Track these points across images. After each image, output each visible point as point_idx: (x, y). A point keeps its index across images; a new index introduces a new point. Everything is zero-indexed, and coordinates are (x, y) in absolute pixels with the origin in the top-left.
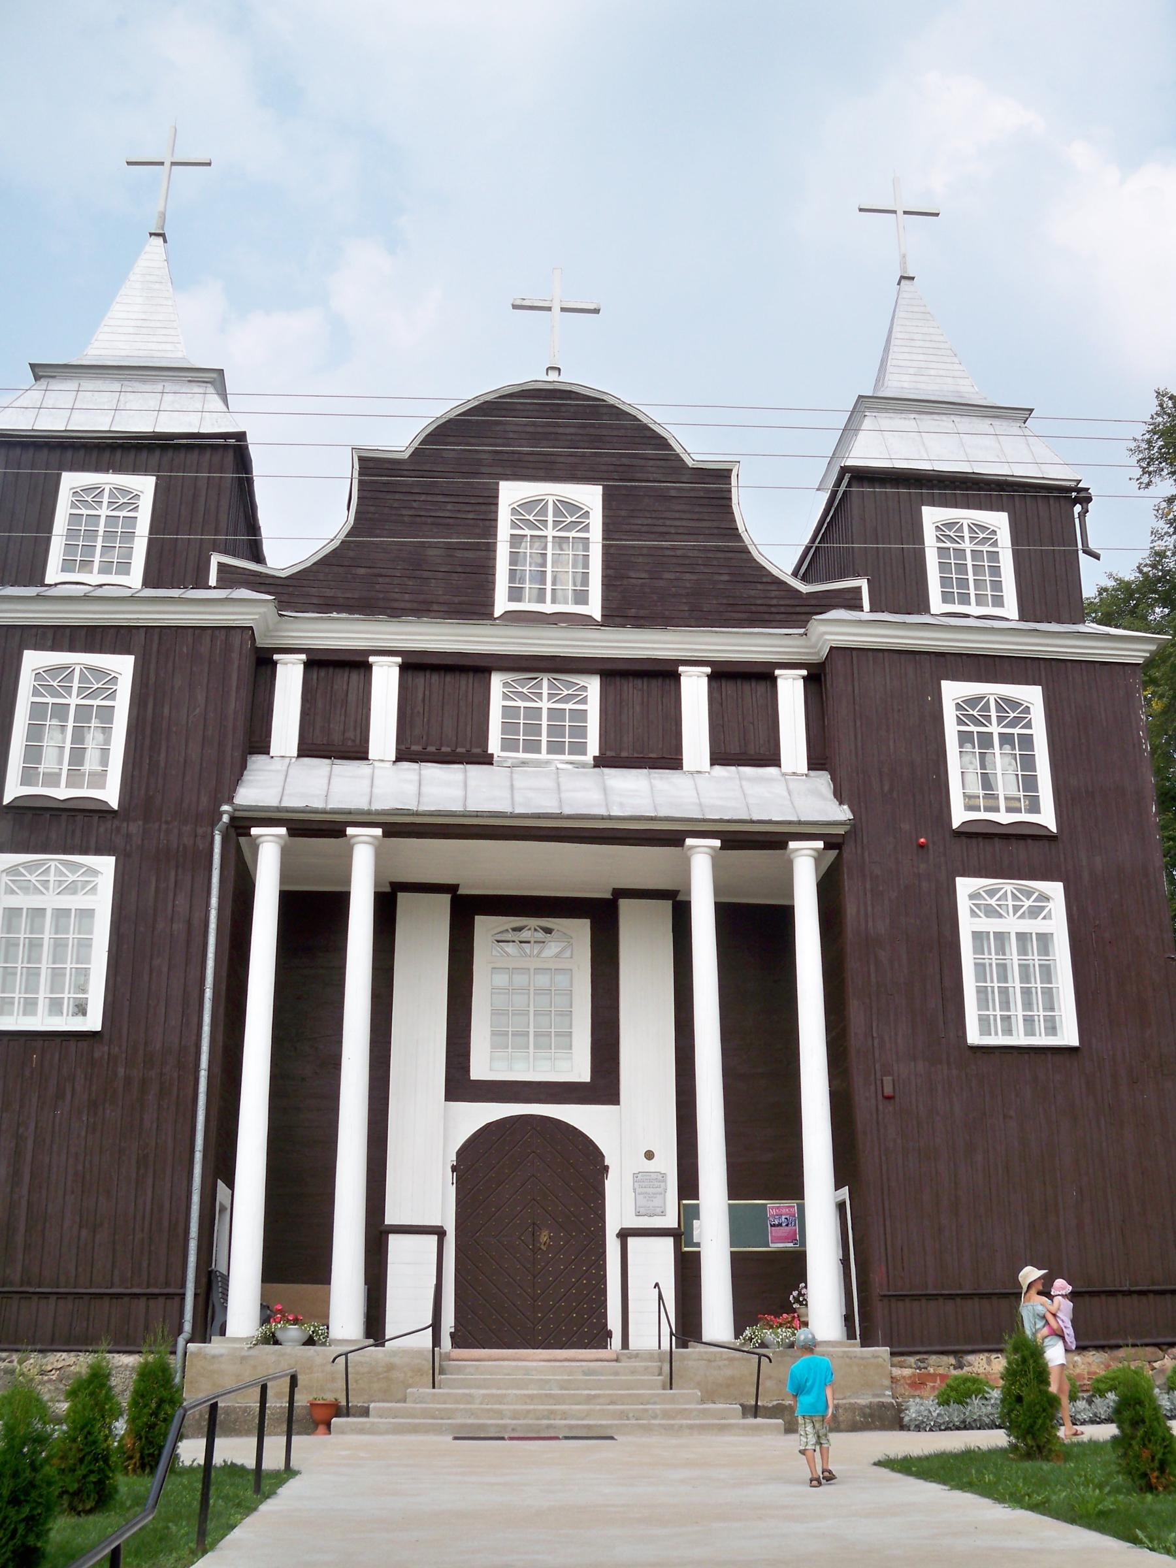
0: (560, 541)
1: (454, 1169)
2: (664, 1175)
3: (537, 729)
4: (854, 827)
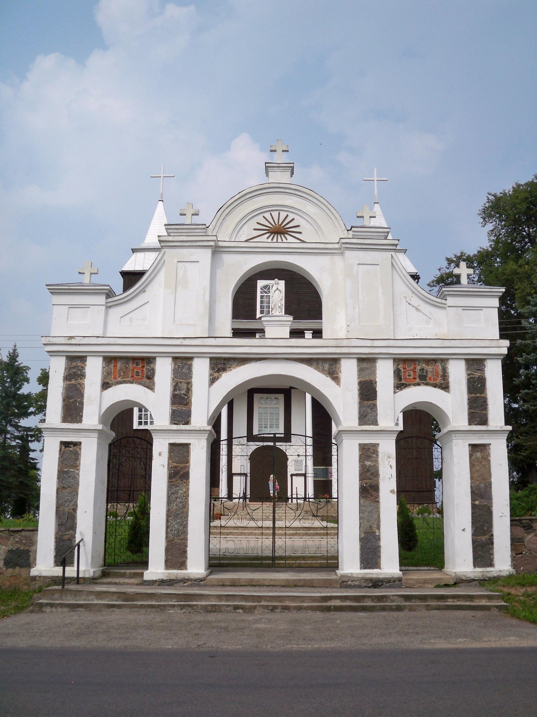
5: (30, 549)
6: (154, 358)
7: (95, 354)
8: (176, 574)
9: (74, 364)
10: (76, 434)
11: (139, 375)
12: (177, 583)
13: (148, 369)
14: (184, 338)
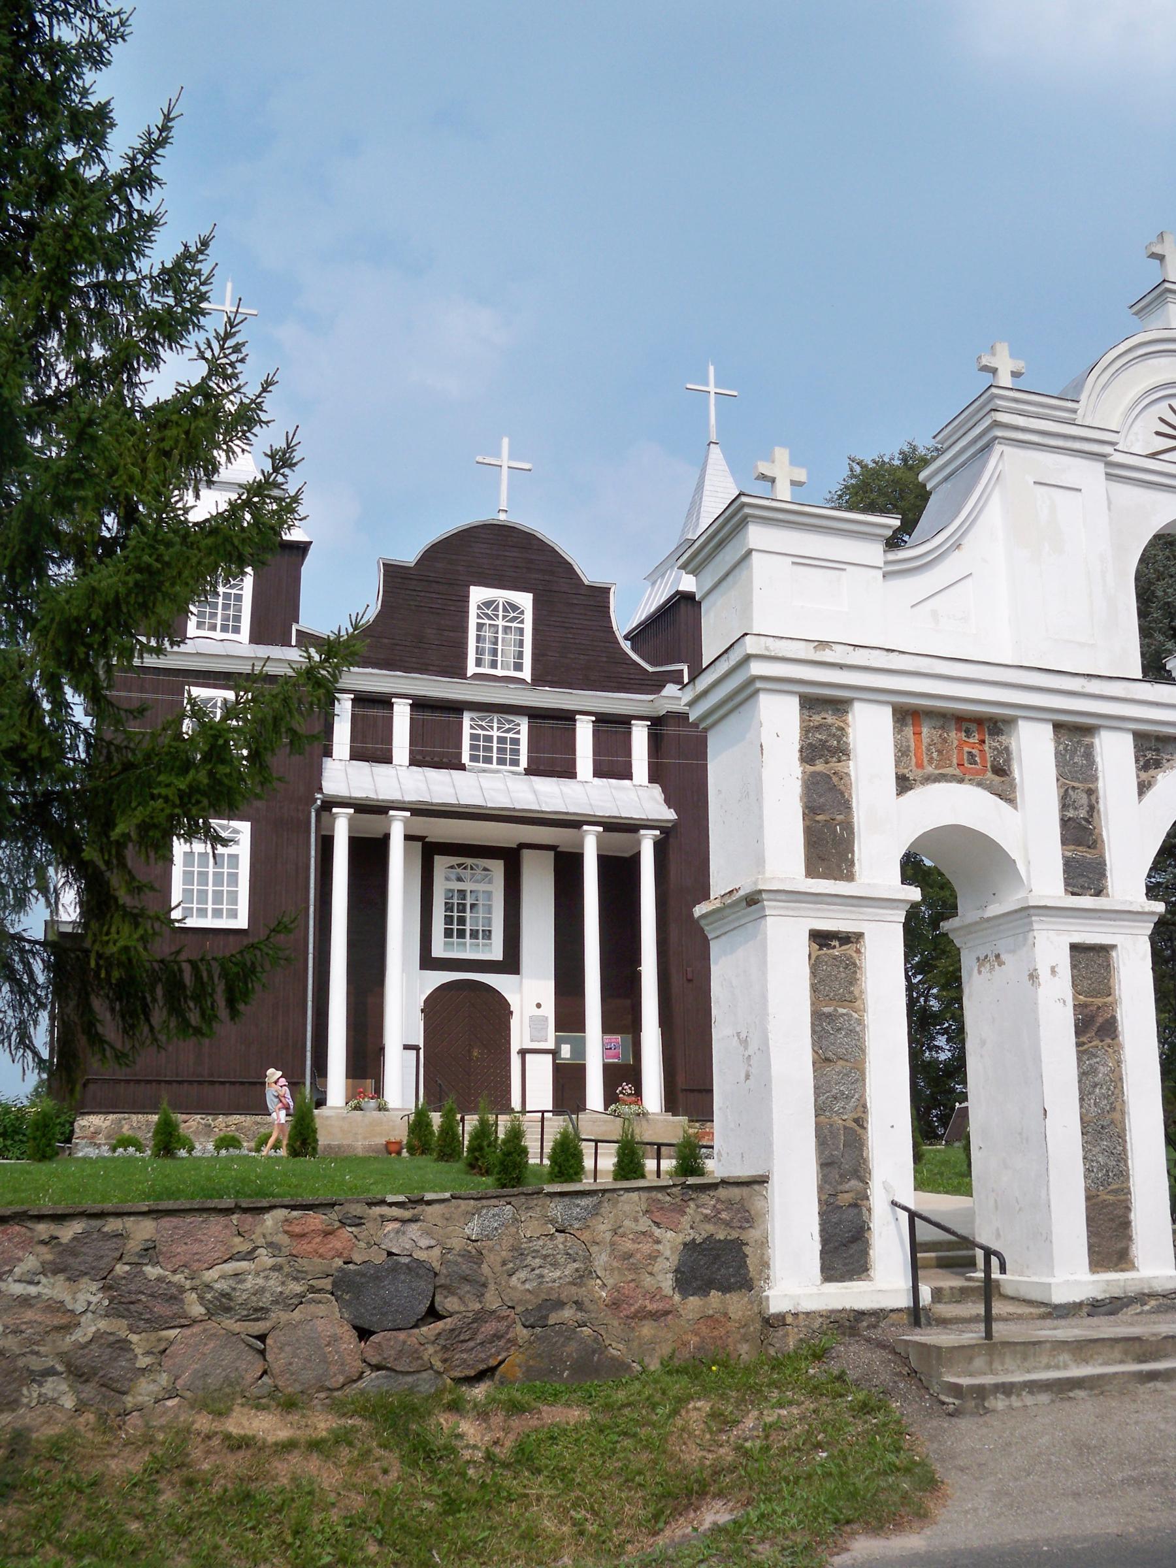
0: (506, 629)
1: (422, 1011)
2: (547, 1018)
3: (490, 749)
4: (676, 824)
5: (744, 1237)
6: (1010, 722)
7: (874, 694)
8: (1122, 1284)
9: (817, 718)
10: (851, 912)
11: (975, 763)
12: (1127, 1306)
13: (996, 749)
14: (1088, 675)
